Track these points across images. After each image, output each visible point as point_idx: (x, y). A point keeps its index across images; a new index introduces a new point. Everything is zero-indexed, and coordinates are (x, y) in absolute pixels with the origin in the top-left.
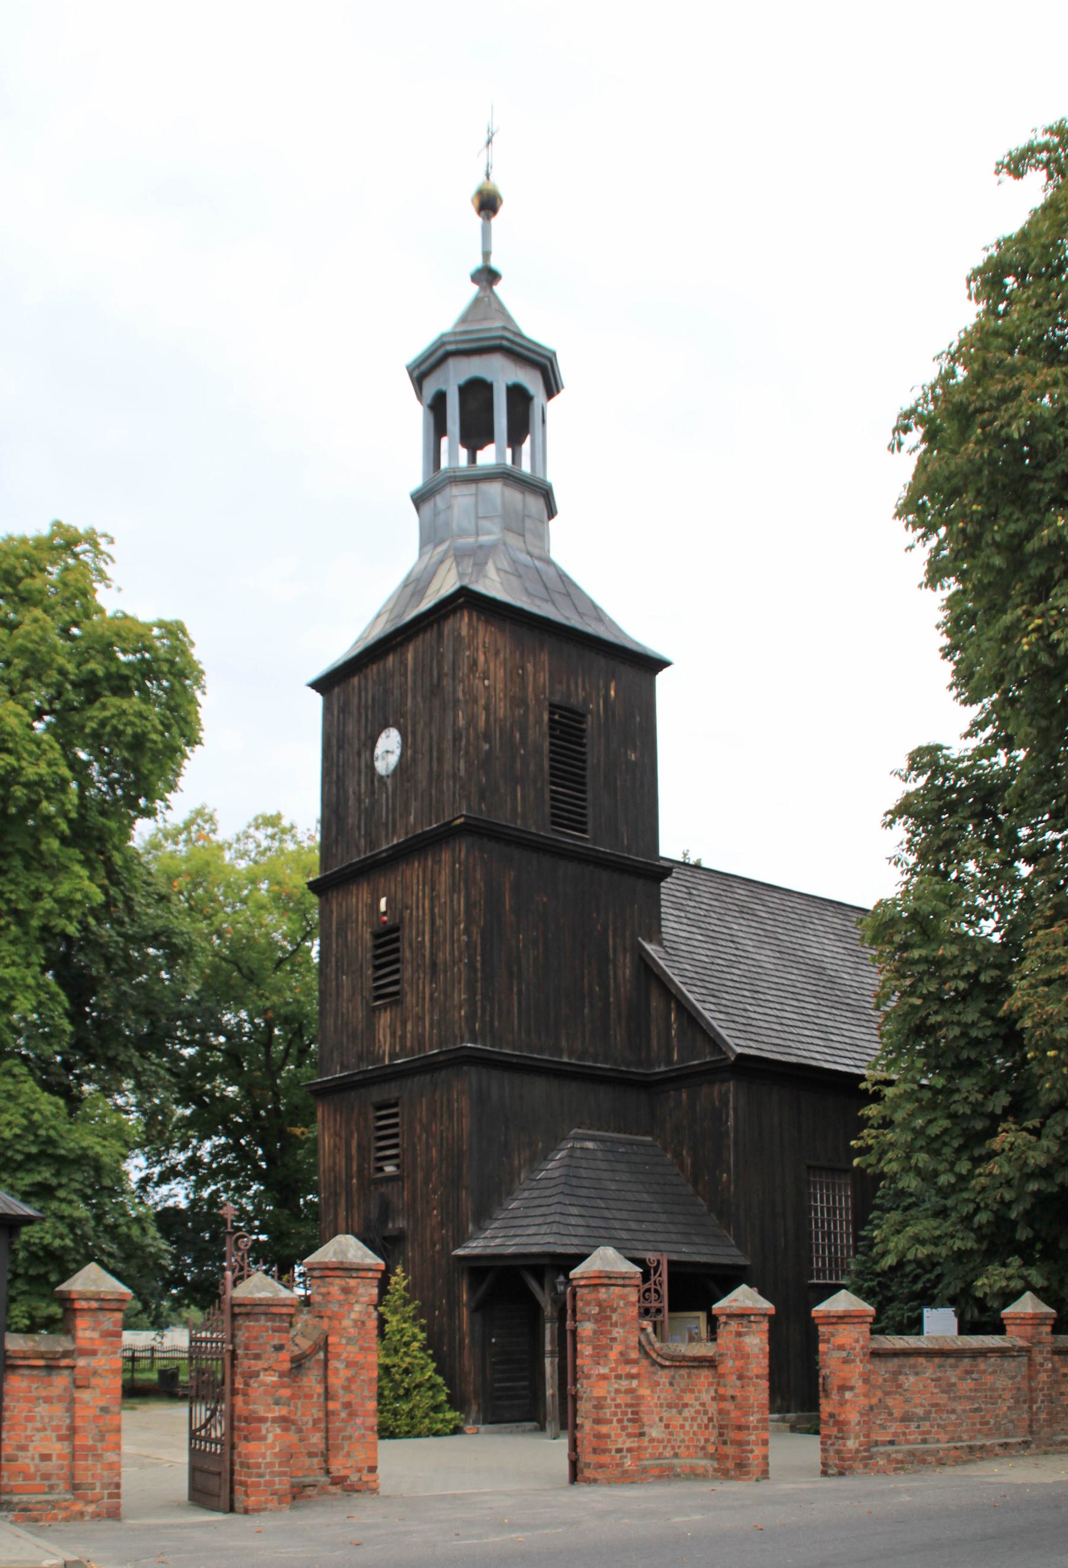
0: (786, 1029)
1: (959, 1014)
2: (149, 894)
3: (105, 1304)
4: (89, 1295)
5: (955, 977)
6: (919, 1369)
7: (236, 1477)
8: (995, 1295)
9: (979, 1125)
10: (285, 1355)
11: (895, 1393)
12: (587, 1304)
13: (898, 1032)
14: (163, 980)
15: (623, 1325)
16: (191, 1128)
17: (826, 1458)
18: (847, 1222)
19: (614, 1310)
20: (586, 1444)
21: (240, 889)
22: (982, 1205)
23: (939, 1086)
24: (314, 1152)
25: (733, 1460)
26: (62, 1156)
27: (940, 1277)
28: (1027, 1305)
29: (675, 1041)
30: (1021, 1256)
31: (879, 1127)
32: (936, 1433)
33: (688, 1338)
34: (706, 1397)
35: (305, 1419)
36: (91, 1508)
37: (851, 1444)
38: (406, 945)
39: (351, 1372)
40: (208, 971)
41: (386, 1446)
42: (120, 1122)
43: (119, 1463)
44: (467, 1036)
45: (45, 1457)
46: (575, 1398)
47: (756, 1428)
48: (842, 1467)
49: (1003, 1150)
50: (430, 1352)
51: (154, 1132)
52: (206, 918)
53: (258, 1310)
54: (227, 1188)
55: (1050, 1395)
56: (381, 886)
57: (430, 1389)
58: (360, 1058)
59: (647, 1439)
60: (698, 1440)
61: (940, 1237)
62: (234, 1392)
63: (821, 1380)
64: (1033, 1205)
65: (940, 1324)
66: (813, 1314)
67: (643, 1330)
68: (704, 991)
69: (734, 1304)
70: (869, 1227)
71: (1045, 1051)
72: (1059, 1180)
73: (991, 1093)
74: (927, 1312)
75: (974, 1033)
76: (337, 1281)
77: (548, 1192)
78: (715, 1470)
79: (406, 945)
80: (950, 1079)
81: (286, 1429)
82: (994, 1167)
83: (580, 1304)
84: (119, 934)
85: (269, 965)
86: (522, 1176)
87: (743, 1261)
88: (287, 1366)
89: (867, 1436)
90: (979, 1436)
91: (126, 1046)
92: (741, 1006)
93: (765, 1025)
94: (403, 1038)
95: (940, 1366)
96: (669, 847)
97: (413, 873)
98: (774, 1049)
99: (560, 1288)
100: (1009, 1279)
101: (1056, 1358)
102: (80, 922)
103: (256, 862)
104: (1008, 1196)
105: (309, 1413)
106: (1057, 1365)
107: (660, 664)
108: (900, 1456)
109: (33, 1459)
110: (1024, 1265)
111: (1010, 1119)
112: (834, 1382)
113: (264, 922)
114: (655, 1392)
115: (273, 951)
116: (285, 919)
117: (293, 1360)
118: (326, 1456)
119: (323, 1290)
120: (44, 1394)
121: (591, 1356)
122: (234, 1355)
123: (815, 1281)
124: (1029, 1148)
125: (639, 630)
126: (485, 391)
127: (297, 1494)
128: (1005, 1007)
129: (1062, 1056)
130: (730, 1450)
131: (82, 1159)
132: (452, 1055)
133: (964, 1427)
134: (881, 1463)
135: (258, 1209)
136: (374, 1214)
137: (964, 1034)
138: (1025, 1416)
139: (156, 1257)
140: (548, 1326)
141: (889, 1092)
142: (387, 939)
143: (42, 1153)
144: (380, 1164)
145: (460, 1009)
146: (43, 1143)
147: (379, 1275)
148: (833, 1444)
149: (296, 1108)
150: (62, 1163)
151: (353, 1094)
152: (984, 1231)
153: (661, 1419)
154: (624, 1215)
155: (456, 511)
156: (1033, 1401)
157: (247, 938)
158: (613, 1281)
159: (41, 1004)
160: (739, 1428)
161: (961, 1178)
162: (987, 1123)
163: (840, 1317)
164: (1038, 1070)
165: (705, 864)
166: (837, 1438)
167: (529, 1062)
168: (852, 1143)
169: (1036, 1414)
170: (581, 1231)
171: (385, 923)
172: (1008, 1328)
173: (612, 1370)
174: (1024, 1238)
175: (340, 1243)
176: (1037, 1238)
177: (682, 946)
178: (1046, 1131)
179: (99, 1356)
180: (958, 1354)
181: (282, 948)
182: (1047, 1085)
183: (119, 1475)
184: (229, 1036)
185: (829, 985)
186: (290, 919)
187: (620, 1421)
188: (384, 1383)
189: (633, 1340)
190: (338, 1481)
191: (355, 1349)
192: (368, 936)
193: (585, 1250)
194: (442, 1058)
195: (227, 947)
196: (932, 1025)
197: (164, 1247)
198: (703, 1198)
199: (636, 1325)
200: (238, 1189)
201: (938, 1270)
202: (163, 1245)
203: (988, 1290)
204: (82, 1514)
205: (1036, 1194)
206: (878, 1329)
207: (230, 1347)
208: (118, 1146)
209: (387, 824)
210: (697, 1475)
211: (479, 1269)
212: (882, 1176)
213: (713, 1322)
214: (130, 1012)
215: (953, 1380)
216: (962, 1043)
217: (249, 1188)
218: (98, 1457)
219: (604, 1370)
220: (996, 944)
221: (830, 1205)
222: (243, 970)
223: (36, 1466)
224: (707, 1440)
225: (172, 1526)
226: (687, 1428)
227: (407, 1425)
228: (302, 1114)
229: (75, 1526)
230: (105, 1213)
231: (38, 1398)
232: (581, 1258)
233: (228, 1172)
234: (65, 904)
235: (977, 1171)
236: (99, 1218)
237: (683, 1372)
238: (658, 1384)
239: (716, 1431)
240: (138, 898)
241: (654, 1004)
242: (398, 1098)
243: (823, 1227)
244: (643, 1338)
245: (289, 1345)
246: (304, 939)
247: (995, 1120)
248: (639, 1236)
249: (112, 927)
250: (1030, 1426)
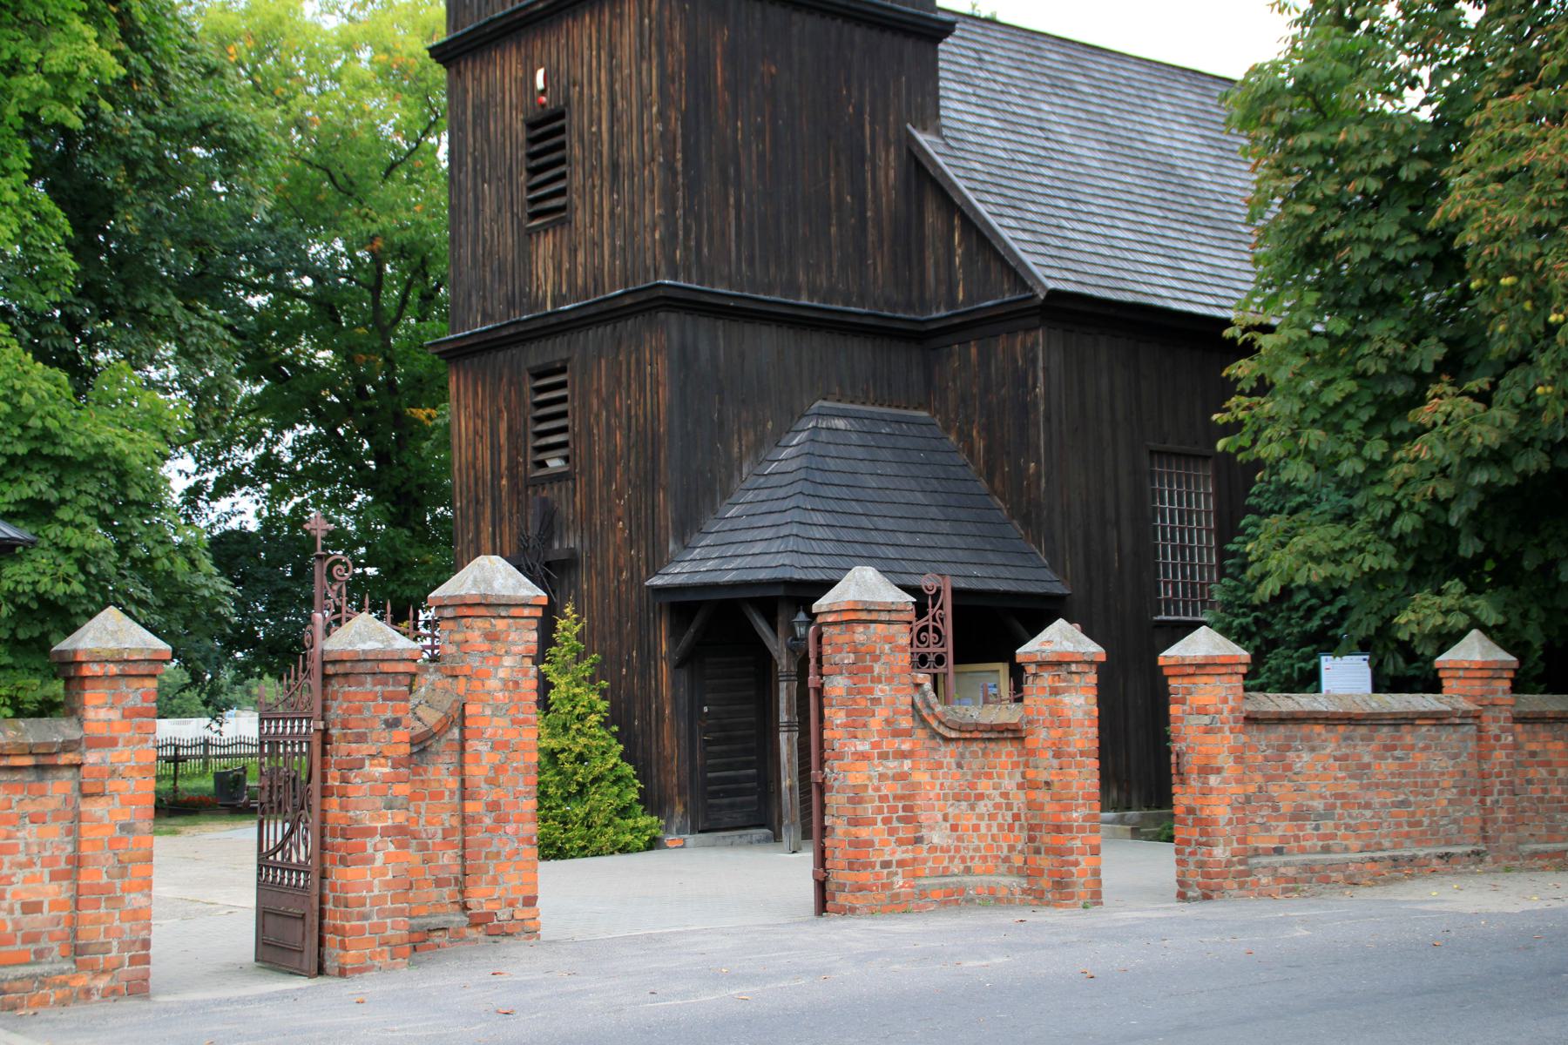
0: (1118, 253)
1: (1370, 226)
2: (190, 65)
3: (129, 668)
4: (105, 655)
5: (1363, 173)
6: (1317, 743)
7: (328, 921)
8: (1426, 637)
9: (1400, 389)
10: (402, 734)
11: (1282, 777)
12: (838, 648)
13: (1280, 256)
14: (218, 195)
15: (890, 680)
16: (265, 415)
17: (1183, 873)
18: (1209, 531)
19: (876, 659)
20: (837, 859)
21: (329, 58)
22: (1404, 504)
23: (1340, 332)
24: (445, 444)
25: (1049, 878)
26: (68, 458)
27: (1344, 611)
28: (1474, 650)
30: (1464, 580)
31: (1252, 394)
32: (1345, 838)
33: (983, 698)
34: (1009, 784)
35: (431, 829)
36: (102, 983)
37: (1220, 853)
38: (575, 139)
39: (498, 757)
40: (284, 180)
41: (544, 866)
42: (154, 403)
43: (149, 908)
44: (663, 269)
45: (31, 908)
46: (822, 789)
47: (1081, 829)
48: (1207, 887)
49: (1435, 424)
50: (615, 728)
51: (208, 419)
52: (279, 101)
53: (361, 668)
54: (317, 500)
55: (1511, 783)
57: (614, 783)
58: (511, 304)
59: (925, 847)
60: (1000, 848)
61: (1342, 551)
62: (326, 792)
63: (1173, 758)
64: (1481, 505)
65: (1345, 677)
66: (1161, 662)
67: (918, 686)
68: (1000, 200)
69: (1047, 648)
70: (1238, 539)
71: (1497, 279)
72: (1518, 469)
73: (1417, 341)
74: (1326, 662)
75: (1390, 254)
76: (479, 623)
77: (781, 493)
78: (1024, 892)
79: (575, 139)
80: (1355, 322)
81: (402, 846)
82: (1426, 449)
83: (827, 650)
84: (147, 125)
85: (377, 171)
86: (745, 470)
87: (1059, 589)
88: (404, 749)
89: (1241, 841)
90: (1407, 843)
91: (162, 292)
92: (1054, 221)
93: (1089, 248)
94: (572, 273)
95: (1347, 738)
98: (1101, 282)
99: (800, 631)
100: (1447, 612)
101: (1519, 728)
102: (84, 108)
103: (351, 19)
104: (1444, 491)
105: (437, 819)
106: (1521, 739)
108: (1291, 872)
109: (11, 911)
110: (1467, 592)
111: (1445, 378)
112: (1191, 761)
113: (367, 108)
114: (936, 776)
115: (379, 151)
116: (398, 103)
117: (413, 742)
118: (461, 884)
119: (458, 637)
120: (32, 808)
121: (845, 725)
122: (325, 737)
123: (1163, 617)
124: (1473, 421)
127: (420, 943)
128: (1438, 215)
129: (1523, 285)
130: (1044, 861)
131: (96, 462)
132: (643, 297)
133: (1385, 831)
134: (1264, 881)
135: (364, 528)
136: (532, 532)
137: (1375, 256)
138: (1475, 813)
139: (211, 604)
140: (783, 685)
141: (1266, 341)
142: (548, 130)
143: (34, 454)
144: (540, 457)
145: (653, 231)
146: (36, 438)
147: (539, 613)
148: (1193, 853)
149: (420, 380)
150: (64, 465)
151: (501, 355)
152: (1408, 543)
153: (945, 819)
154: (890, 524)
156: (1486, 792)
157: (343, 132)
158: (874, 616)
159: (25, 229)
160: (1058, 829)
161: (1373, 466)
162: (1412, 385)
163: (1198, 666)
164: (1485, 307)
165: (1001, 18)
166: (1199, 844)
168: (1215, 417)
169: (1492, 811)
170: (829, 547)
171: (543, 106)
172: (1445, 683)
173: (874, 745)
174: (1470, 555)
175: (482, 567)
176: (1489, 552)
177: (972, 133)
178: (1498, 396)
179: (120, 748)
180: (1372, 720)
181: (394, 146)
182: (1501, 328)
183: (148, 927)
184: (318, 280)
185: (1180, 190)
186: (405, 104)
187: (886, 821)
188: (546, 777)
189: (904, 703)
190: (478, 921)
191: (506, 722)
192: (519, 126)
193: (832, 575)
194: (628, 301)
195: (311, 145)
196: (1329, 244)
197: (223, 588)
198: (1002, 499)
199: (907, 679)
200: (333, 501)
201: (1342, 601)
202: (223, 585)
203: (1415, 629)
204: (88, 992)
205: (1486, 488)
206: (1255, 679)
207: (321, 725)
208: (150, 441)
210: (998, 900)
211: (685, 606)
212: (1258, 464)
213: (1017, 672)
214: (168, 242)
215: (1367, 759)
216: (1373, 269)
217: (352, 498)
218: (114, 901)
219: (863, 747)
220: (1424, 123)
221: (1184, 505)
222: (336, 180)
223: (16, 923)
224: (1011, 848)
225: (229, 1001)
226: (983, 830)
227: (582, 838)
228: (427, 389)
229: (77, 1012)
230: (133, 540)
231: (22, 817)
232: (828, 585)
233: (319, 476)
234: (63, 82)
235: (1397, 456)
236: (122, 549)
237: (975, 747)
238: (940, 765)
239: (1025, 834)
240: (173, 70)
241: (929, 220)
242: (568, 360)
243: (1173, 539)
244: (917, 699)
245: (408, 719)
246: (425, 133)
247: (1422, 380)
248: (910, 553)
249: (135, 114)
250: (1483, 829)
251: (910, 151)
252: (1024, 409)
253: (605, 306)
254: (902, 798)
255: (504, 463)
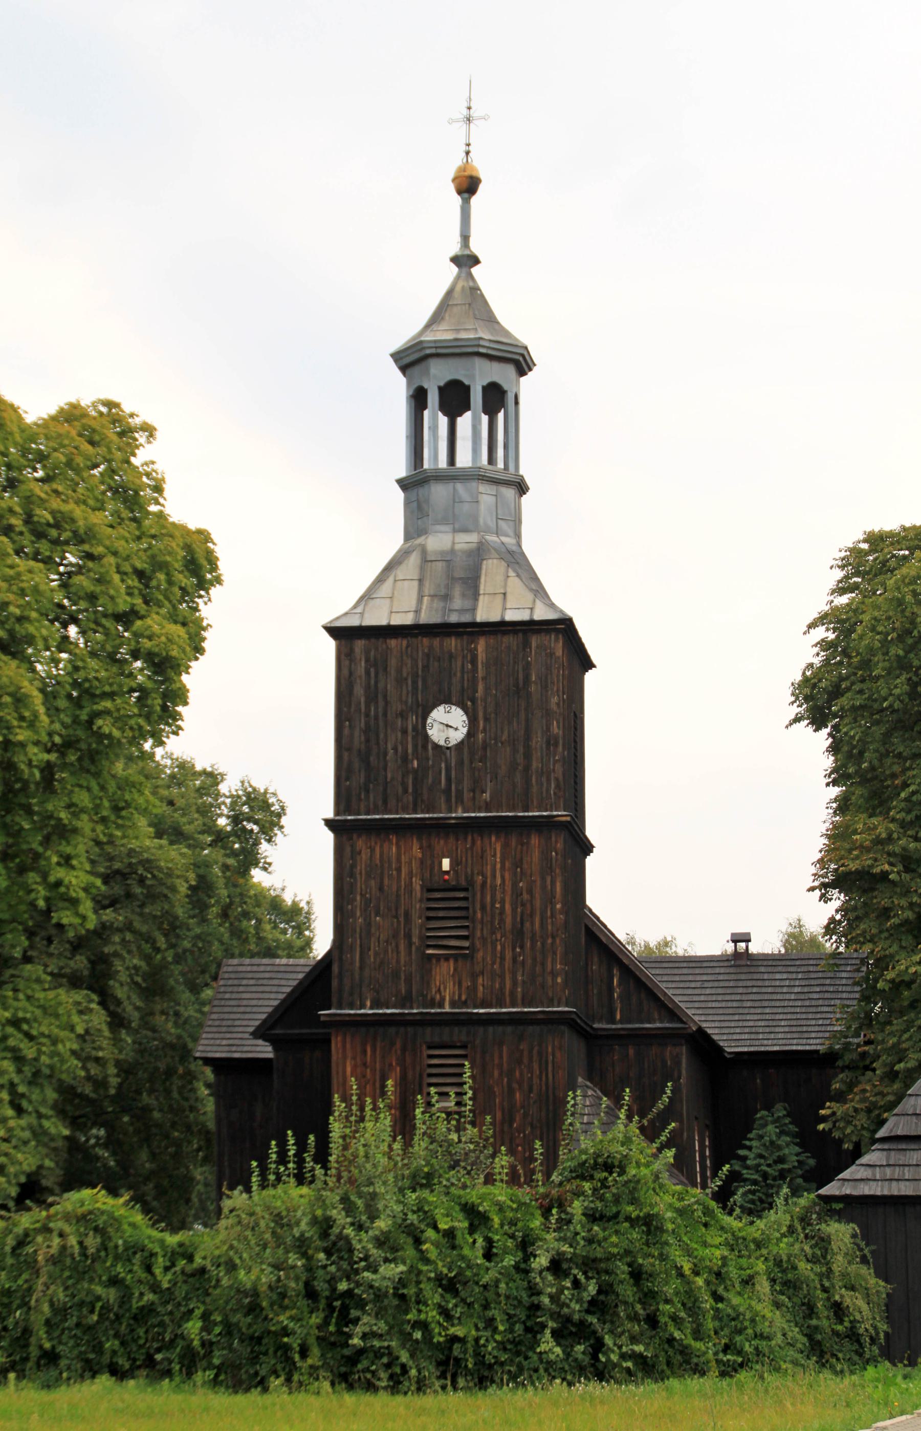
29: (618, 1005)
126: (462, 374)
167: (338, 1018)
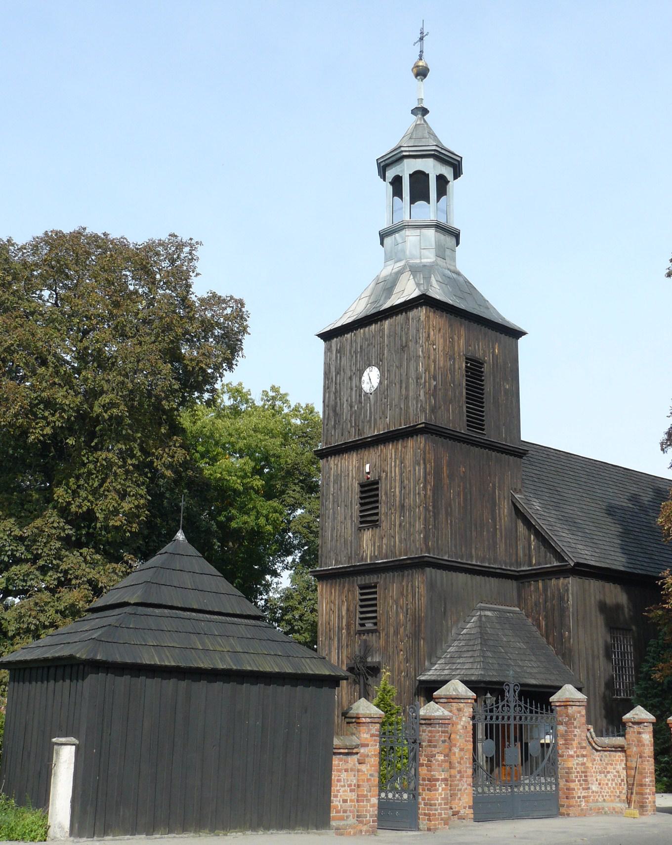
15: (579, 728)
19: (575, 719)
44: (424, 549)
45: (345, 801)
56: (365, 458)
58: (350, 558)
67: (588, 730)
94: (380, 547)
96: (524, 437)
97: (390, 450)
107: (517, 334)
125: (511, 316)
155: (408, 244)
171: (368, 478)
173: (575, 752)
187: (579, 781)
209: (370, 421)
219: (571, 753)
224: (621, 792)
242: (377, 583)
251: (513, 502)
252: (563, 611)
253: (397, 563)
254: (582, 772)
255: (344, 624)
